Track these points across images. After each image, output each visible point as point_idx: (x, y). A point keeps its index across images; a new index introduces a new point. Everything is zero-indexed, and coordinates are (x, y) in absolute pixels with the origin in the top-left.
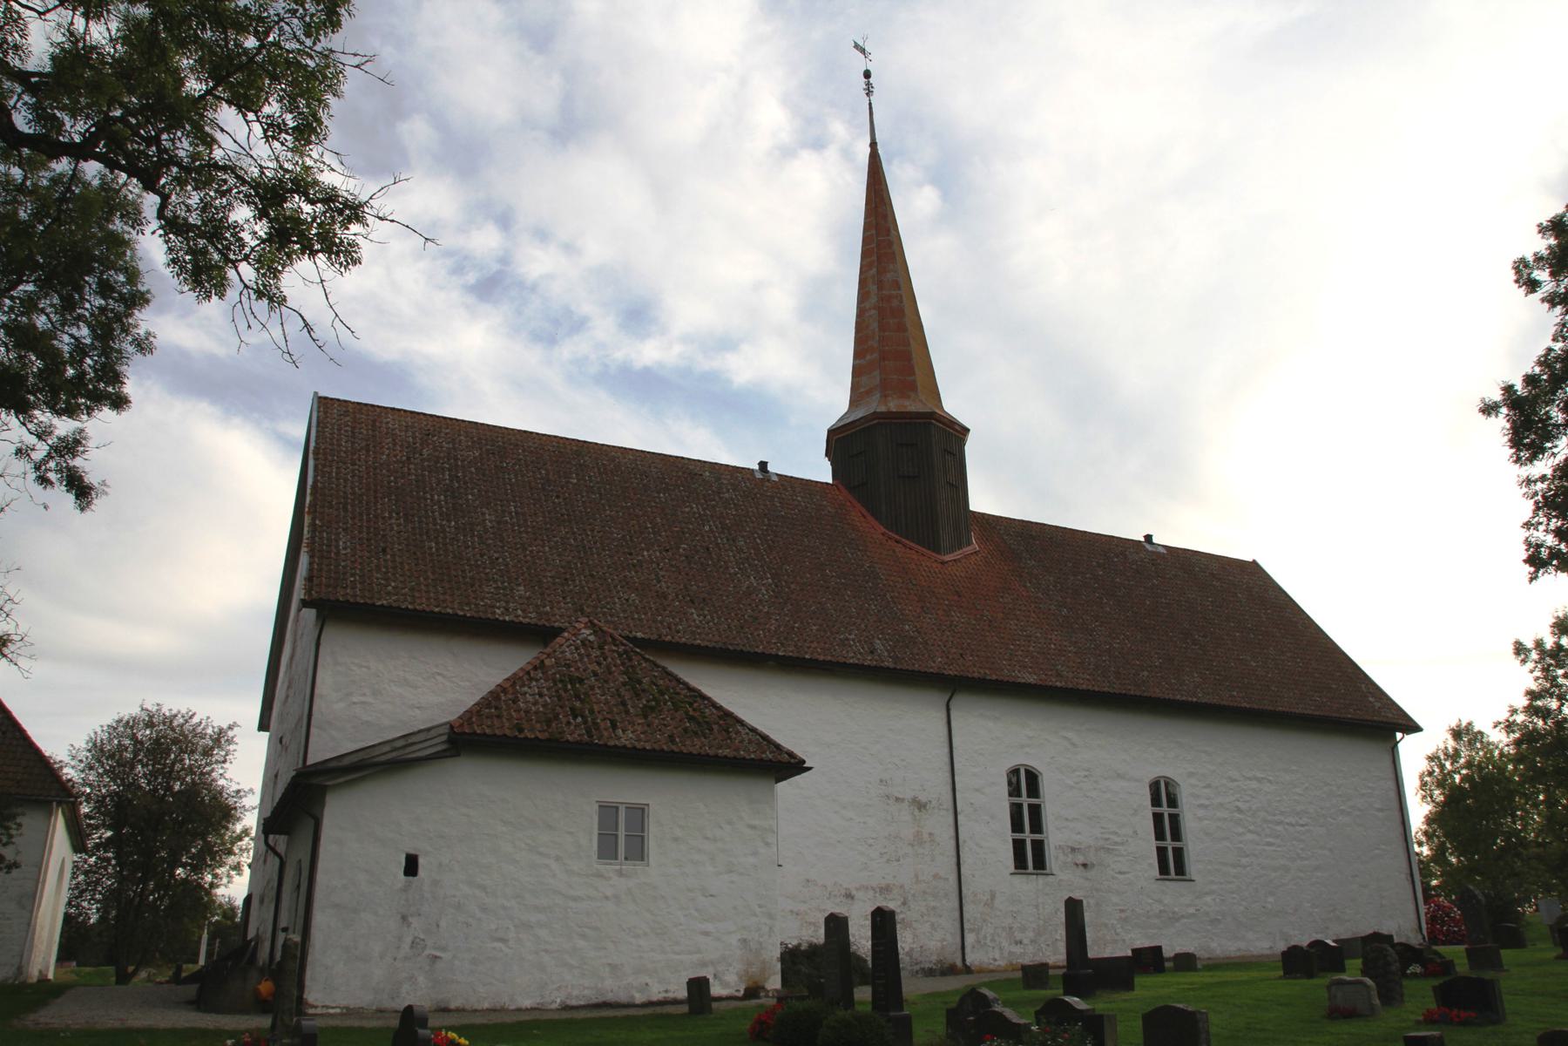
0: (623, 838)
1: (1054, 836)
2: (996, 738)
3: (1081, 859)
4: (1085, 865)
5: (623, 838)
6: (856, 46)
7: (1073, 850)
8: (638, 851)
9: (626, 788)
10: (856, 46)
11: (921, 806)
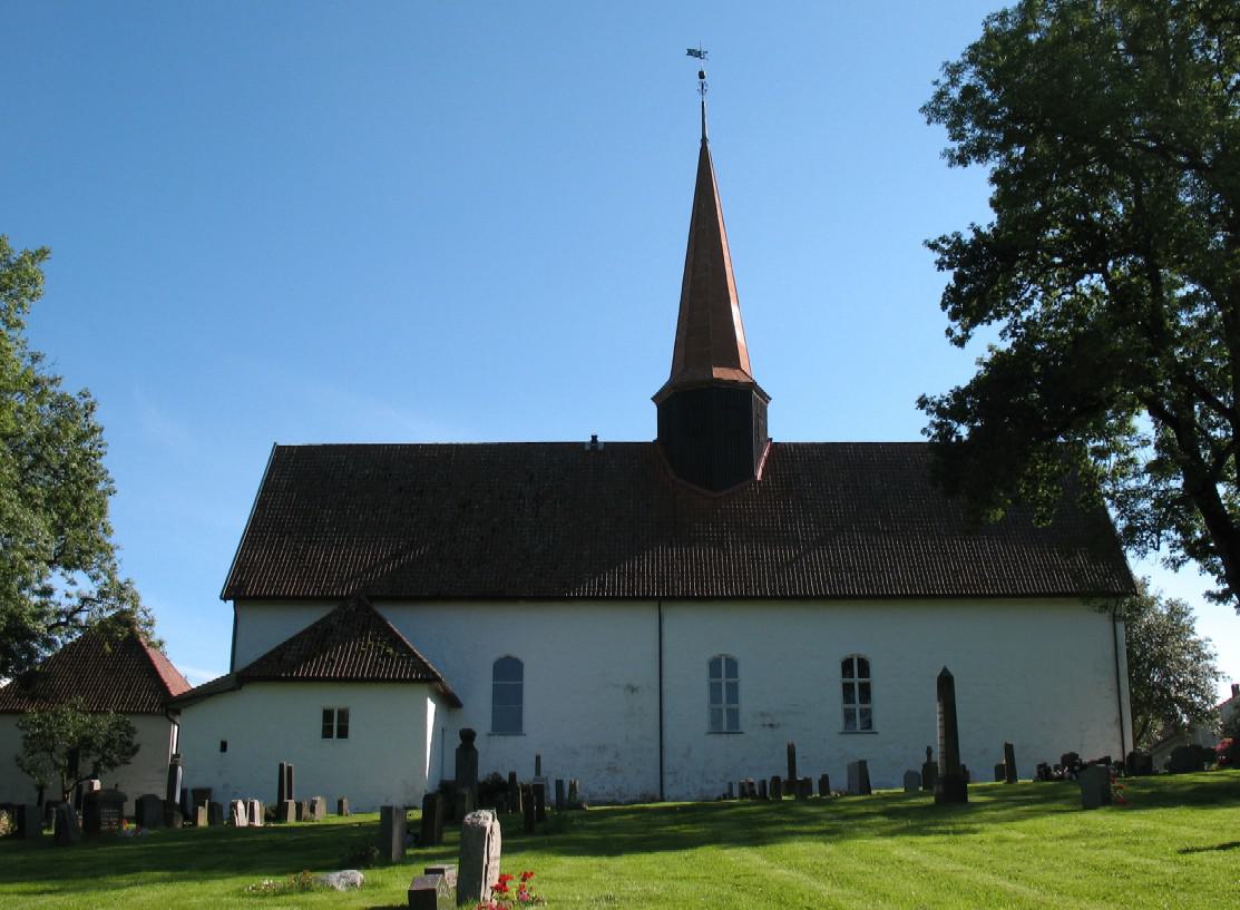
0: (335, 725)
1: (748, 704)
2: (699, 634)
3: (768, 720)
4: (771, 725)
5: (335, 725)
6: (690, 52)
7: (762, 714)
8: (343, 733)
9: (335, 698)
10: (690, 52)
11: (633, 690)
